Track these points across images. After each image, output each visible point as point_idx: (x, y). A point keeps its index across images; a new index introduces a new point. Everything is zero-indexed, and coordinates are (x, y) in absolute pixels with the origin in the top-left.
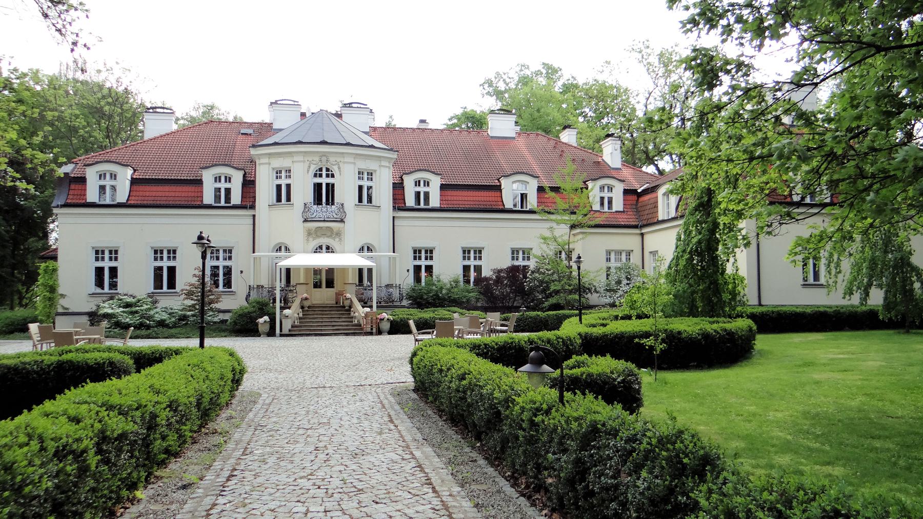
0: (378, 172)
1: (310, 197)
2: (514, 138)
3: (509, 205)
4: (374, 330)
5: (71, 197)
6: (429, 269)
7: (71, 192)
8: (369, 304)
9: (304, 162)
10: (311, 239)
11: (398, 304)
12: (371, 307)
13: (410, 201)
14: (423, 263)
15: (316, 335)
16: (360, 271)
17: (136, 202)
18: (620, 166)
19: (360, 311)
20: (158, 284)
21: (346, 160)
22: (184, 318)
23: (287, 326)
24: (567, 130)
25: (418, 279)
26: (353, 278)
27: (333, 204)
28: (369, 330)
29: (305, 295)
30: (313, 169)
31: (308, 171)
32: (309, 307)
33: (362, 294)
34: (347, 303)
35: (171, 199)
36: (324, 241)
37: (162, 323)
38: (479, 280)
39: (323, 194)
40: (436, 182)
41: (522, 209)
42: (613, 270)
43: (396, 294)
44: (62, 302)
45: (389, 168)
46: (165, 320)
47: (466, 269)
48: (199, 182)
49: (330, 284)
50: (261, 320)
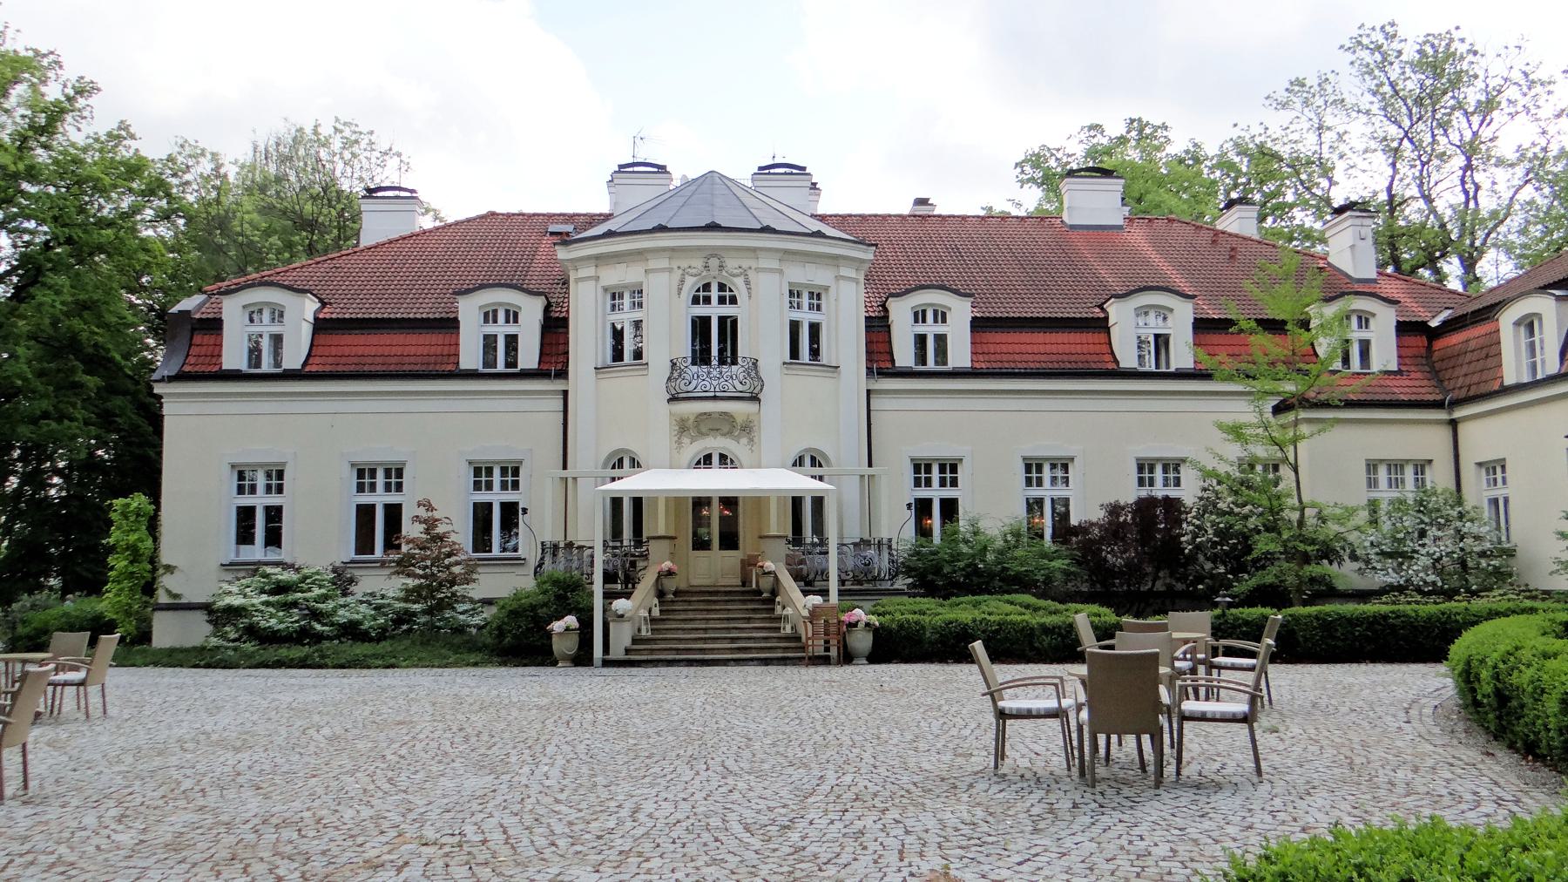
0: (832, 291)
1: (683, 346)
2: (1120, 227)
3: (1128, 360)
4: (833, 652)
5: (192, 360)
6: (949, 508)
7: (194, 350)
8: (818, 585)
9: (670, 270)
10: (686, 440)
11: (887, 585)
12: (824, 593)
13: (904, 355)
14: (936, 493)
15: (690, 663)
16: (797, 502)
17: (320, 368)
18: (1374, 275)
19: (798, 603)
20: (364, 542)
21: (763, 263)
22: (404, 618)
23: (622, 638)
24: (1236, 208)
25: (923, 532)
26: (778, 523)
27: (735, 362)
28: (820, 651)
29: (667, 565)
30: (691, 284)
31: (680, 290)
32: (676, 593)
33: (802, 562)
34: (766, 584)
35: (393, 360)
36: (715, 444)
37: (352, 631)
38: (1063, 530)
39: (714, 341)
40: (961, 312)
41: (1157, 372)
42: (1384, 506)
43: (883, 563)
44: (166, 581)
45: (857, 281)
46: (359, 623)
47: (1035, 505)
48: (450, 325)
49: (729, 540)
50: (557, 626)
